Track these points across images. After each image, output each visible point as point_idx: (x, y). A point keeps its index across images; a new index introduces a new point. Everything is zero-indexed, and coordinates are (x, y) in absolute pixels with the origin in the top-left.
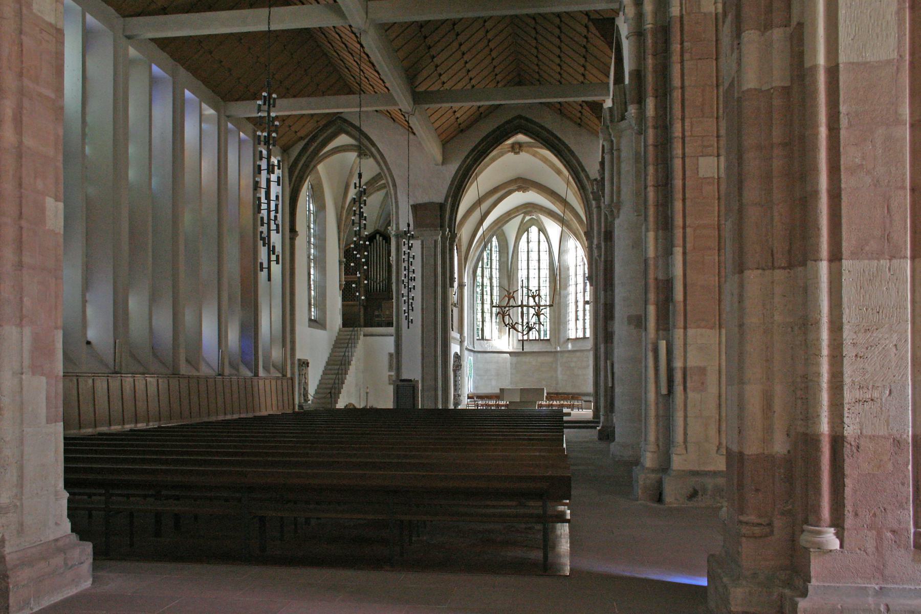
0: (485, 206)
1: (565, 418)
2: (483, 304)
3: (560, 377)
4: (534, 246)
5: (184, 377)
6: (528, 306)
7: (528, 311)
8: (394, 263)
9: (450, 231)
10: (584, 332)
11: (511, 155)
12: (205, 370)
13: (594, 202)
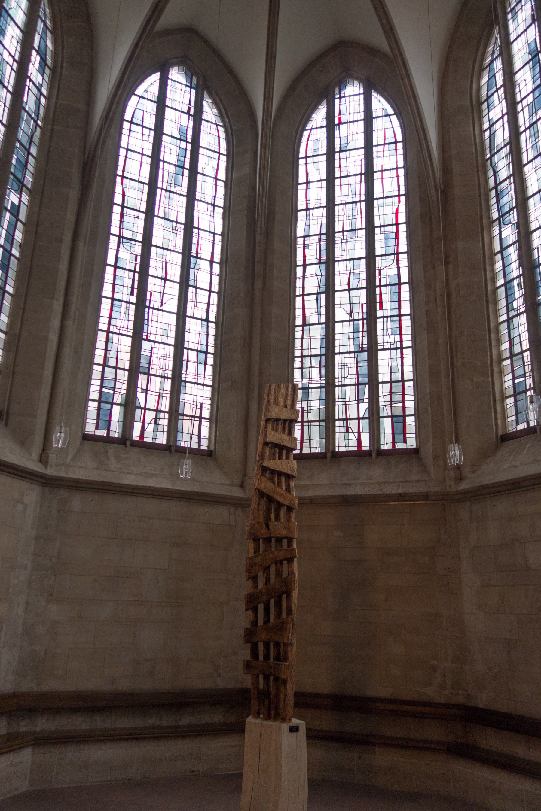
4: (351, 134)
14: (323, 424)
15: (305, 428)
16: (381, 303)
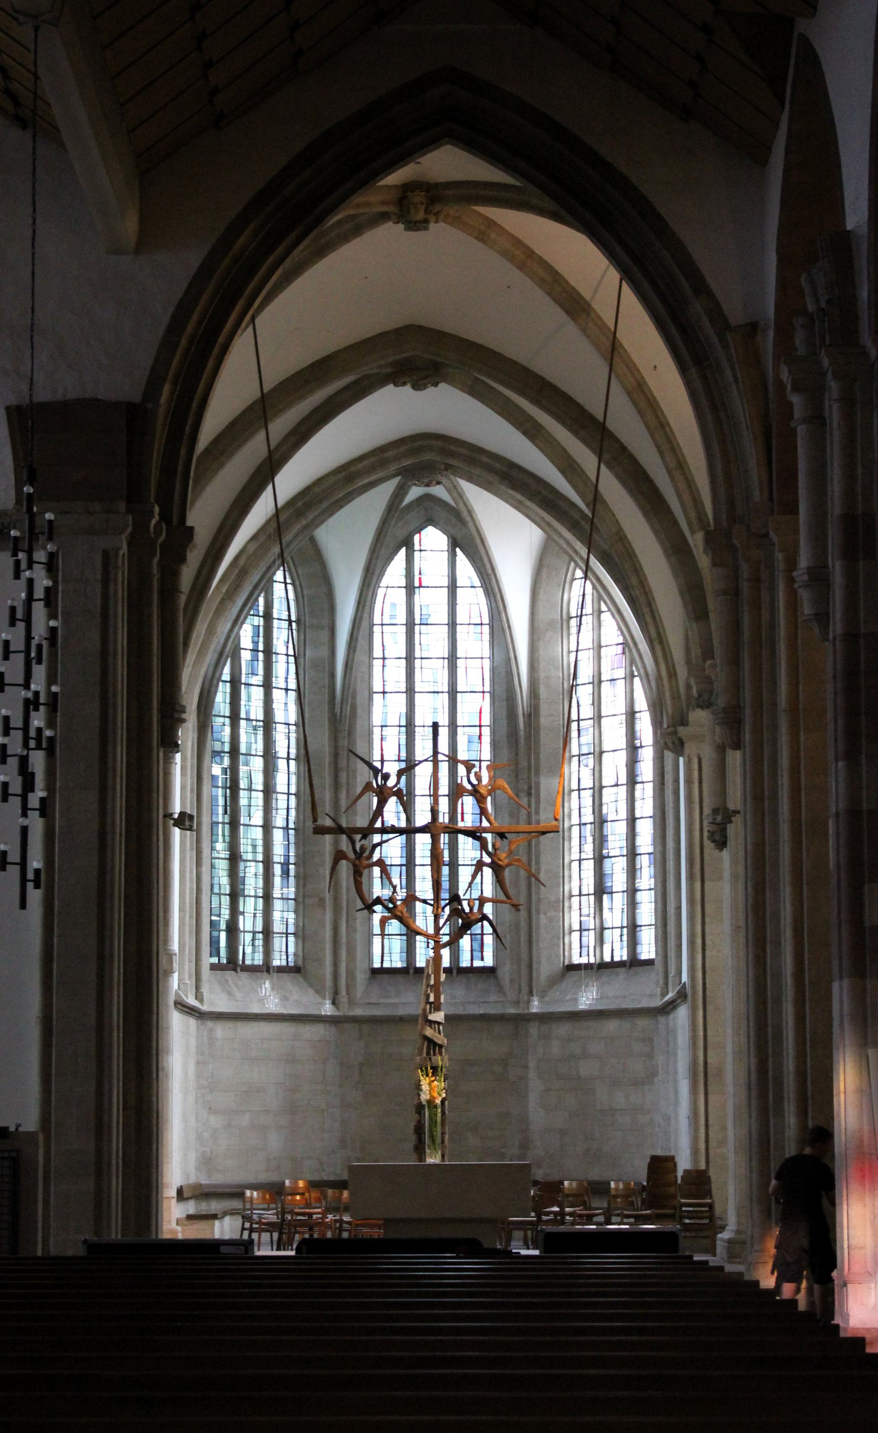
0: (281, 425)
2: (234, 824)
3: (538, 1117)
4: (432, 603)
6: (454, 831)
7: (454, 848)
9: (165, 517)
11: (389, 235)
13: (796, 400)
14: (405, 938)
15: (386, 941)
16: (462, 814)
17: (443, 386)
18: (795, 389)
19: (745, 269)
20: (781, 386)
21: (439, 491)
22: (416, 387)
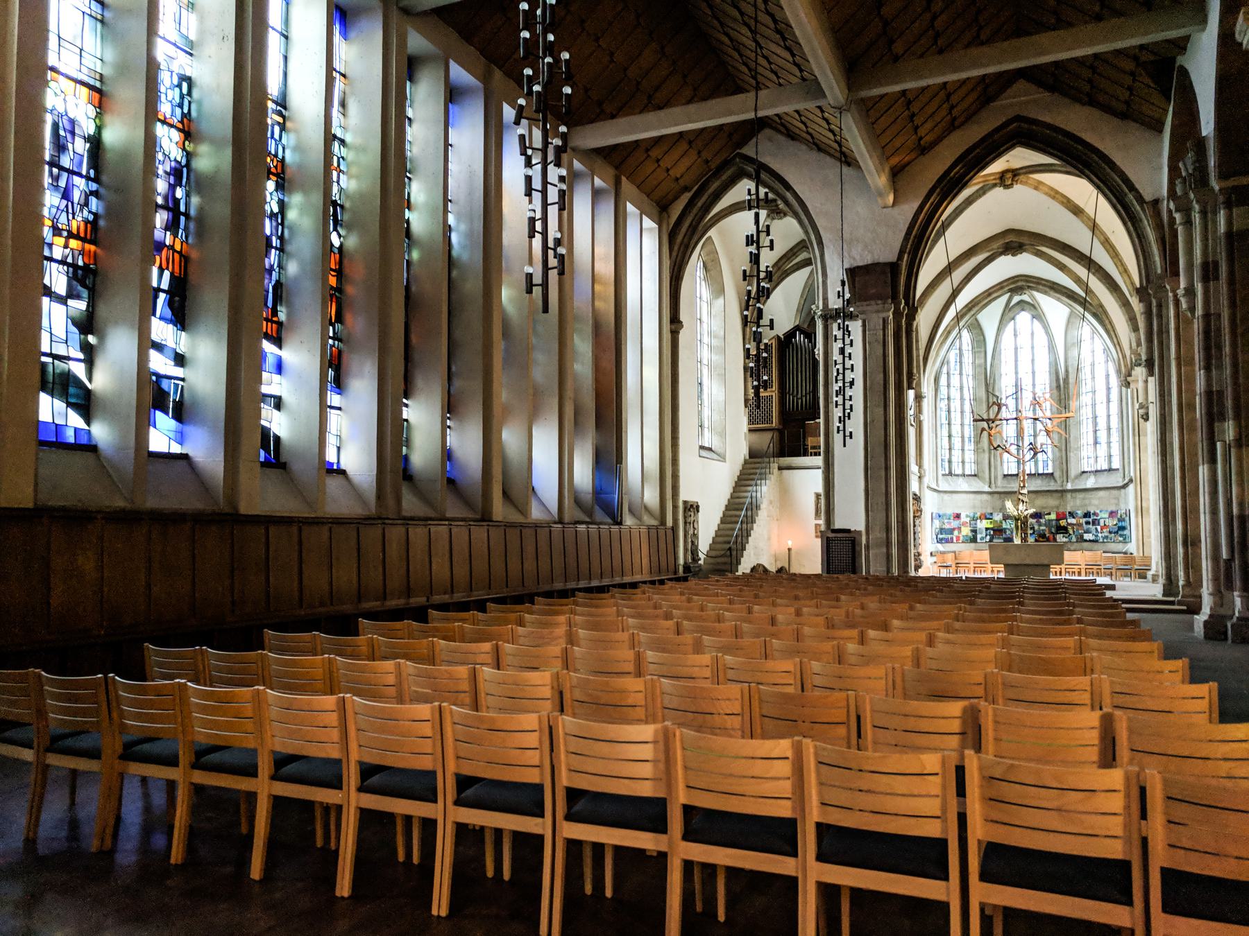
0: (959, 274)
1: (1109, 594)
4: (1024, 340)
5: (498, 524)
8: (821, 359)
9: (907, 304)
10: (1110, 462)
12: (536, 513)
17: (1024, 254)
18: (1177, 211)
19: (1152, 172)
20: (1170, 211)
21: (1025, 297)
22: (1013, 255)
